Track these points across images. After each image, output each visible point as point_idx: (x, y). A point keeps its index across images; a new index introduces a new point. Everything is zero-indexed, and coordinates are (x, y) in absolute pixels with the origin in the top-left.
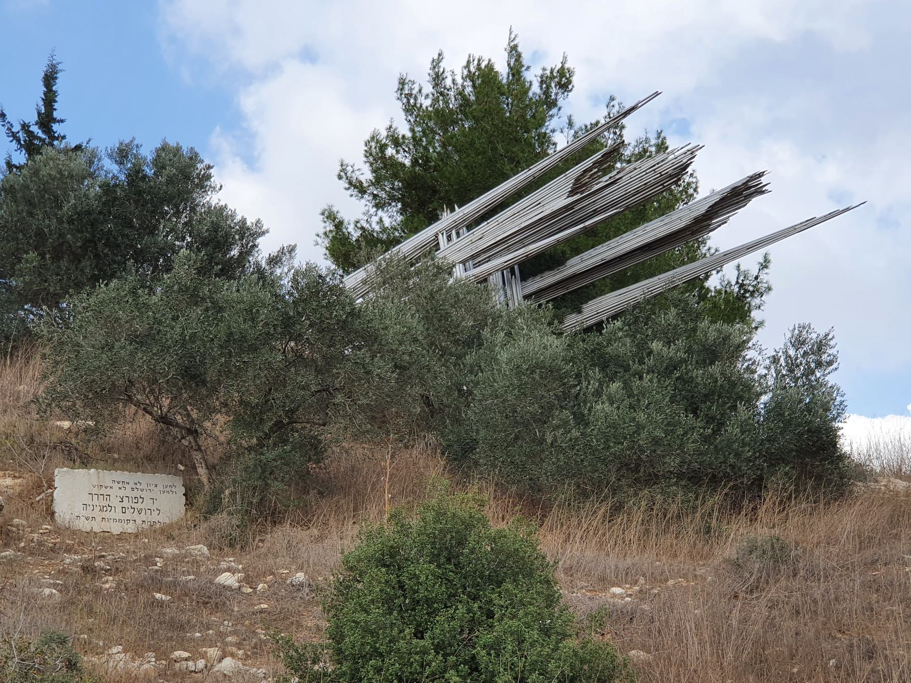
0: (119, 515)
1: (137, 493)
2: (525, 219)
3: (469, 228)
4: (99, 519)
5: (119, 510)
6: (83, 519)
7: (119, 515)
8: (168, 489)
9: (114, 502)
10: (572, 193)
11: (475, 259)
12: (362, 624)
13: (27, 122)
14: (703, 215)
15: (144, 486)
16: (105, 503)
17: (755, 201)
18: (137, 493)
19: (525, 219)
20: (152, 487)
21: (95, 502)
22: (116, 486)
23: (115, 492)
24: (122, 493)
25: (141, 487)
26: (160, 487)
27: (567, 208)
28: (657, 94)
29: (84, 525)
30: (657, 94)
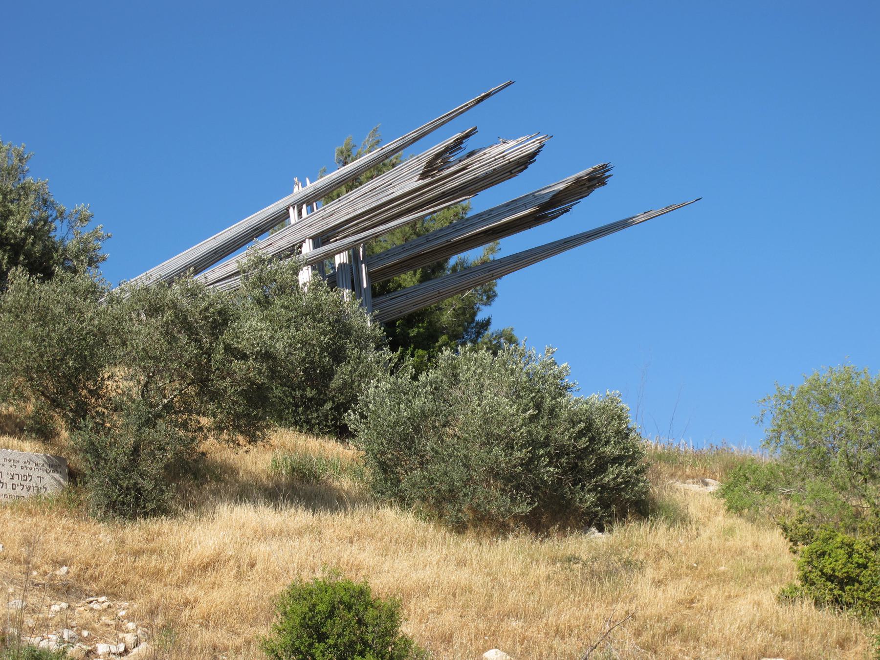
5: (9, 486)
10: (423, 176)
17: (598, 192)
22: (7, 464)
24: (13, 471)
28: (624, 224)
30: (624, 224)
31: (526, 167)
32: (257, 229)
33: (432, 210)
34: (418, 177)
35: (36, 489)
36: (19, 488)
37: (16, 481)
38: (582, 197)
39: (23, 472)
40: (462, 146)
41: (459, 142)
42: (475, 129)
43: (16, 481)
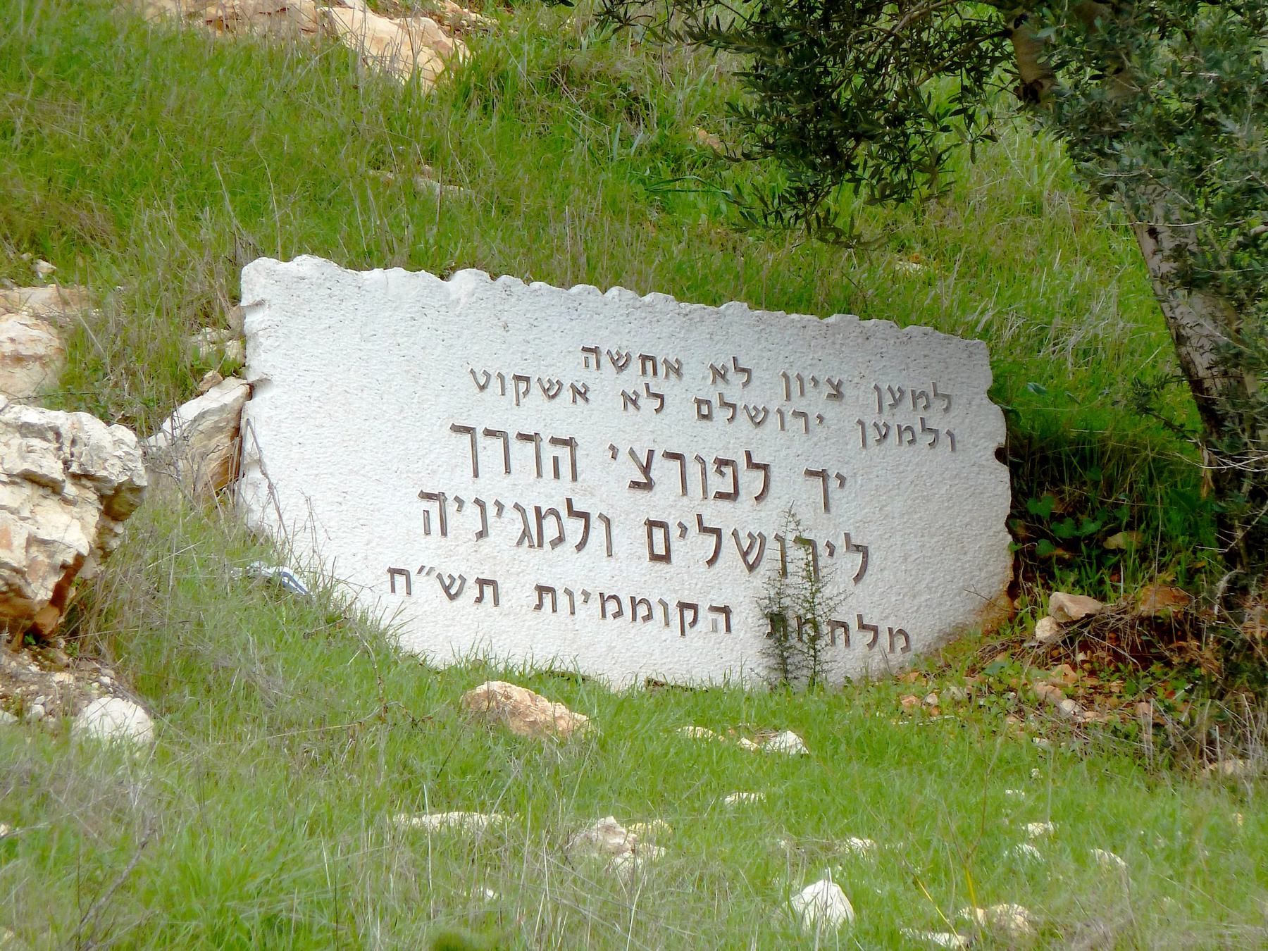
0: (630, 573)
4: (518, 594)
5: (630, 538)
6: (427, 589)
7: (630, 573)
8: (906, 415)
9: (605, 486)
16: (551, 494)
20: (816, 402)
21: (493, 485)
22: (607, 385)
23: (601, 423)
28: (476, 475)
29: (435, 632)
30: (476, 475)
35: (798, 555)
37: (665, 501)
43: (665, 501)
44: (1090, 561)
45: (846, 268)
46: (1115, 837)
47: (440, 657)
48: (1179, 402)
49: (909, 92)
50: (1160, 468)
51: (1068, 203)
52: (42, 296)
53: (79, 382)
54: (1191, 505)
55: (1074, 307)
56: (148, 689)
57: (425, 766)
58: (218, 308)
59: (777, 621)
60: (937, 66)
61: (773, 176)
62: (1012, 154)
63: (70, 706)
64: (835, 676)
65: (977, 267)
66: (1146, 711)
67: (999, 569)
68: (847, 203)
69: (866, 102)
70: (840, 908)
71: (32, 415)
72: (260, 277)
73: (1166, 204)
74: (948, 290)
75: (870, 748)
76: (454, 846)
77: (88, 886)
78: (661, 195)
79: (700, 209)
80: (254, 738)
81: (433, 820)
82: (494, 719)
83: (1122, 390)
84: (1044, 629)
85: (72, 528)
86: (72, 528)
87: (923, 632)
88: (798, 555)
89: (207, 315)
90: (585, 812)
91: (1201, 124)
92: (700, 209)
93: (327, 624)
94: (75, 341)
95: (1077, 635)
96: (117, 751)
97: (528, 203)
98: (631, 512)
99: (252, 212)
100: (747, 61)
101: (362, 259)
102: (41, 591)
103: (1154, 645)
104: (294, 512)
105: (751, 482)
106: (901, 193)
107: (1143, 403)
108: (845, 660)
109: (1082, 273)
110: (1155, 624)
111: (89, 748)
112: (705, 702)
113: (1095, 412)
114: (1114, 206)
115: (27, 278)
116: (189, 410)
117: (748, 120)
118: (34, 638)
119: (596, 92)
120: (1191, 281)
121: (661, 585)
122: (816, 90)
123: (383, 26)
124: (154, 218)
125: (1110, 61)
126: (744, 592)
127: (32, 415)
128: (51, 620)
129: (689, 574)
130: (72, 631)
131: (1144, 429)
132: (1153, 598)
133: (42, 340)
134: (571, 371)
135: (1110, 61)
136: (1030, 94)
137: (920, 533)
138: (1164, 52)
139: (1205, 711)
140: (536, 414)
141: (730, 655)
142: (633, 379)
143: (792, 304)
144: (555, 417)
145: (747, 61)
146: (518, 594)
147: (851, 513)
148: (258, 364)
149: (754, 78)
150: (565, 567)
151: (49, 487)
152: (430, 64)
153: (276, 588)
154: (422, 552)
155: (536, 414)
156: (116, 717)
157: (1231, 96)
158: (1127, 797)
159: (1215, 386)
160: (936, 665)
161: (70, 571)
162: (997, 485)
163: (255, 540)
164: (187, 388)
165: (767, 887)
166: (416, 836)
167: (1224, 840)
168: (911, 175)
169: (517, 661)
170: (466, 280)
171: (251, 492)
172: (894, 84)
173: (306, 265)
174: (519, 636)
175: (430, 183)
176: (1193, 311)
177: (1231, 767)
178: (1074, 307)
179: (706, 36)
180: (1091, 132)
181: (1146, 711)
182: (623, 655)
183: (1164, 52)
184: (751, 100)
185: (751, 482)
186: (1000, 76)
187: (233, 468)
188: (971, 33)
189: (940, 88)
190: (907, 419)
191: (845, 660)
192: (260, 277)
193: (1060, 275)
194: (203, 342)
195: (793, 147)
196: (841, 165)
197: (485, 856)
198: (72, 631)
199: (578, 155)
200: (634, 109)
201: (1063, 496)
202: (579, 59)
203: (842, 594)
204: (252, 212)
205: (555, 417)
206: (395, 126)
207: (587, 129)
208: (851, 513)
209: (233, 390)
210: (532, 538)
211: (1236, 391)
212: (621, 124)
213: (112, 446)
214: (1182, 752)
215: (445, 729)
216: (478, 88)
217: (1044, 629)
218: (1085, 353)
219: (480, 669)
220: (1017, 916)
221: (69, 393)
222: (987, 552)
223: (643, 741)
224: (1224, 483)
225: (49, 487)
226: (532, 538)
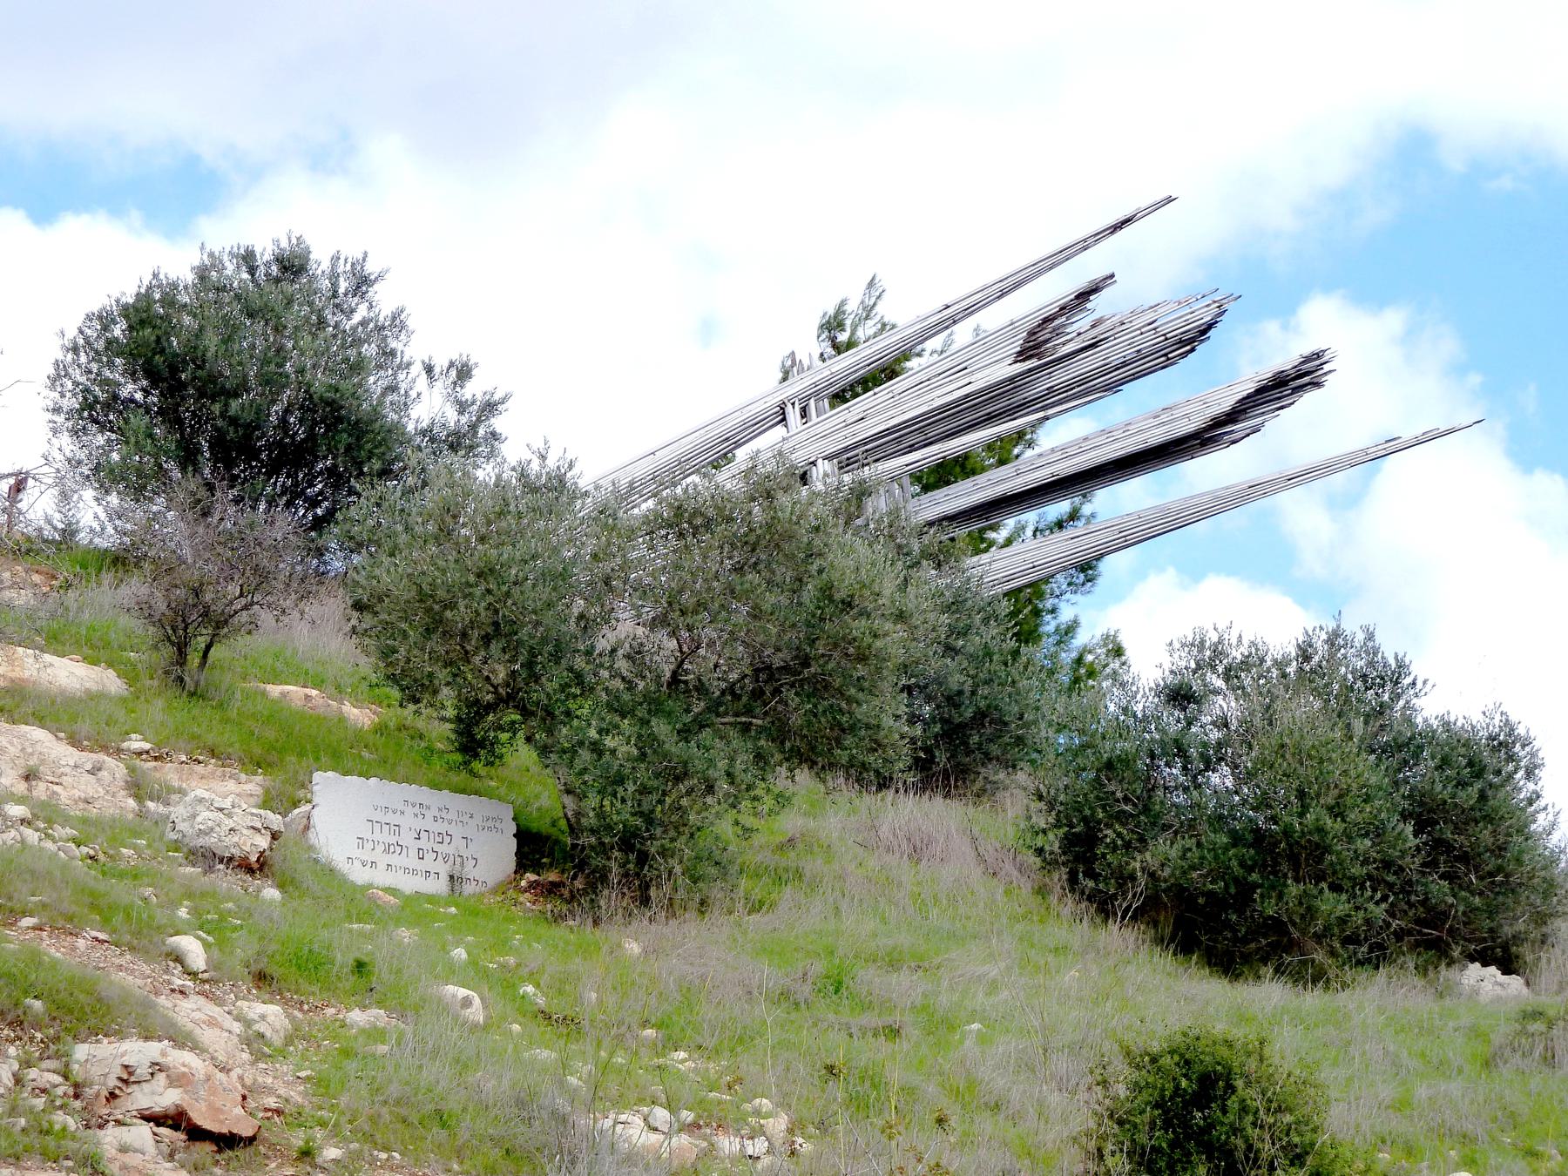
0: (413, 862)
1: (441, 827)
2: (939, 392)
3: (839, 398)
4: (382, 866)
5: (413, 853)
6: (357, 864)
7: (413, 862)
8: (490, 823)
9: (407, 838)
10: (1022, 355)
11: (846, 459)
12: (1062, 798)
13: (1521, 731)
14: (1228, 414)
15: (452, 815)
16: (393, 839)
17: (1309, 399)
18: (441, 827)
19: (939, 392)
20: (466, 818)
21: (377, 836)
22: (409, 810)
23: (409, 822)
24: (419, 824)
25: (449, 816)
26: (478, 820)
27: (1011, 379)
28: (1170, 200)
29: (359, 875)
30: (1170, 200)
31: (1193, 350)
32: (727, 439)
33: (1041, 414)
34: (1011, 359)
35: (458, 860)
36: (430, 857)
37: (423, 843)
38: (1282, 408)
39: (437, 827)
40: (1089, 305)
41: (1084, 296)
42: (1112, 276)
43: (423, 843)
44: (537, 867)
45: (476, 783)
46: (538, 940)
47: (360, 883)
48: (563, 824)
49: (496, 737)
50: (557, 842)
51: (535, 769)
52: (259, 778)
53: (268, 802)
54: (564, 851)
55: (537, 797)
56: (281, 886)
57: (354, 912)
58: (305, 784)
59: (452, 877)
60: (503, 730)
61: (458, 757)
62: (521, 755)
63: (259, 891)
64: (466, 893)
65: (511, 785)
66: (549, 907)
67: (512, 866)
68: (477, 766)
69: (484, 739)
70: (464, 956)
71: (254, 811)
72: (318, 776)
73: (563, 771)
74: (503, 790)
75: (475, 913)
76: (361, 934)
77: (261, 938)
78: (427, 760)
79: (438, 764)
80: (309, 901)
81: (355, 926)
82: (373, 900)
83: (548, 820)
84: (523, 883)
85: (263, 842)
86: (263, 842)
87: (491, 883)
88: (458, 860)
89: (303, 786)
90: (397, 926)
91: (573, 752)
92: (438, 764)
93: (330, 872)
94: (267, 791)
95: (532, 885)
96: (272, 901)
97: (391, 761)
98: (414, 846)
99: (317, 759)
100: (453, 726)
101: (345, 774)
102: (253, 858)
103: (552, 890)
104: (322, 840)
105: (447, 839)
106: (492, 764)
107: (554, 824)
108: (469, 889)
109: (539, 788)
110: (551, 883)
111: (264, 901)
112: (431, 898)
113: (540, 825)
114: (548, 771)
115: (255, 774)
116: (296, 811)
117: (452, 742)
118: (250, 870)
119: (411, 732)
120: (568, 792)
121: (421, 866)
122: (471, 736)
123: (355, 711)
124: (291, 759)
125: (550, 732)
126: (444, 869)
127: (254, 811)
128: (256, 866)
129: (429, 863)
130: (261, 869)
131: (553, 831)
132: (552, 876)
133: (259, 791)
134: (401, 807)
135: (550, 732)
136: (529, 739)
137: (494, 855)
138: (564, 731)
139: (565, 908)
140: (390, 818)
141: (439, 886)
142: (417, 810)
143: (463, 791)
144: (395, 819)
145: (453, 726)
146: (382, 866)
147: (473, 850)
148: (316, 800)
149: (455, 731)
150: (395, 859)
151: (258, 830)
152: (367, 722)
153: (316, 861)
154: (356, 853)
155: (390, 818)
156: (271, 893)
157: (581, 743)
158: (544, 930)
159: (573, 820)
160: (494, 891)
161: (262, 853)
162: (513, 844)
163: (311, 848)
164: (296, 804)
165: (445, 950)
166: (351, 931)
167: (567, 943)
168: (495, 758)
169: (381, 884)
170: (373, 780)
171: (311, 834)
172: (492, 734)
173: (330, 774)
174: (382, 878)
175: (365, 754)
176: (569, 801)
177: (571, 923)
178: (537, 797)
179: (443, 719)
180: (544, 751)
181: (549, 907)
182: (409, 884)
183: (564, 731)
184: (453, 737)
185: (447, 839)
186: (521, 734)
187: (307, 828)
188: (513, 722)
189: (504, 736)
190: (490, 824)
191: (469, 889)
192: (318, 776)
193: (532, 788)
194: (301, 793)
195: (780, 453)
196: (476, 756)
197: (368, 937)
198: (261, 869)
199: (405, 749)
200: (421, 737)
201: (532, 847)
202: (408, 723)
203: (470, 871)
204: (317, 759)
205: (395, 819)
206: (358, 739)
207: (408, 741)
208: (473, 850)
209: (309, 806)
210: (387, 851)
211: (578, 821)
212: (418, 741)
213: (275, 821)
214: (558, 918)
215: (361, 903)
216: (380, 729)
217: (523, 883)
218: (539, 809)
219: (370, 886)
220: (512, 960)
221: (265, 805)
222: (510, 863)
223: (414, 908)
224: (574, 846)
225: (258, 830)
226: (387, 851)
